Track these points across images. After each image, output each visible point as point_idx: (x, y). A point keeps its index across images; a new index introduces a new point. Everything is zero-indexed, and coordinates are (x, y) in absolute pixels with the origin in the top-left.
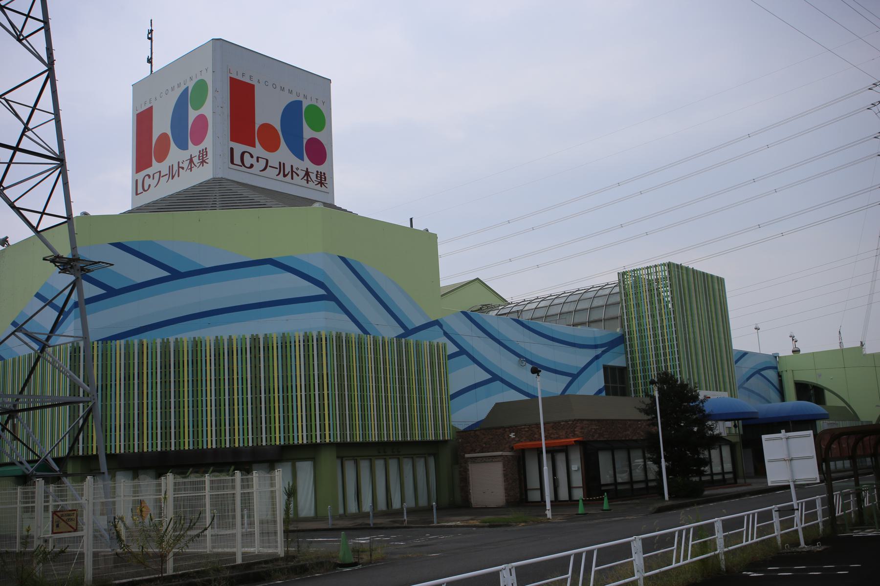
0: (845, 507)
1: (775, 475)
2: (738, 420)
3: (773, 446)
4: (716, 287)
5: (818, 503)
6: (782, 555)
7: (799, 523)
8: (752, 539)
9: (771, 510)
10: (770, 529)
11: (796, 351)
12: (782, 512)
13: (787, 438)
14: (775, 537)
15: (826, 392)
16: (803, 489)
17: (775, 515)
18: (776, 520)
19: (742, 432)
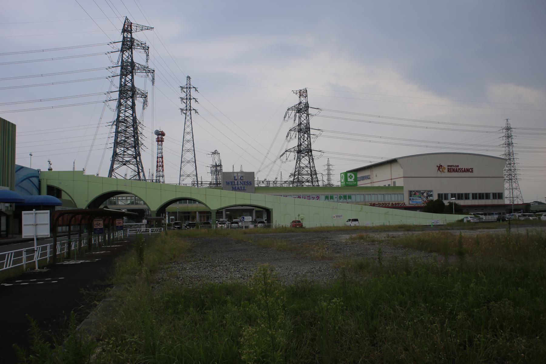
0: (62, 249)
1: (27, 232)
2: (13, 203)
3: (27, 217)
4: (11, 129)
5: (48, 247)
6: (26, 274)
7: (37, 257)
8: (9, 266)
9: (22, 251)
10: (21, 260)
11: (50, 169)
12: (28, 252)
13: (36, 214)
14: (23, 265)
16: (41, 240)
17: (24, 253)
18: (24, 256)
19: (14, 209)
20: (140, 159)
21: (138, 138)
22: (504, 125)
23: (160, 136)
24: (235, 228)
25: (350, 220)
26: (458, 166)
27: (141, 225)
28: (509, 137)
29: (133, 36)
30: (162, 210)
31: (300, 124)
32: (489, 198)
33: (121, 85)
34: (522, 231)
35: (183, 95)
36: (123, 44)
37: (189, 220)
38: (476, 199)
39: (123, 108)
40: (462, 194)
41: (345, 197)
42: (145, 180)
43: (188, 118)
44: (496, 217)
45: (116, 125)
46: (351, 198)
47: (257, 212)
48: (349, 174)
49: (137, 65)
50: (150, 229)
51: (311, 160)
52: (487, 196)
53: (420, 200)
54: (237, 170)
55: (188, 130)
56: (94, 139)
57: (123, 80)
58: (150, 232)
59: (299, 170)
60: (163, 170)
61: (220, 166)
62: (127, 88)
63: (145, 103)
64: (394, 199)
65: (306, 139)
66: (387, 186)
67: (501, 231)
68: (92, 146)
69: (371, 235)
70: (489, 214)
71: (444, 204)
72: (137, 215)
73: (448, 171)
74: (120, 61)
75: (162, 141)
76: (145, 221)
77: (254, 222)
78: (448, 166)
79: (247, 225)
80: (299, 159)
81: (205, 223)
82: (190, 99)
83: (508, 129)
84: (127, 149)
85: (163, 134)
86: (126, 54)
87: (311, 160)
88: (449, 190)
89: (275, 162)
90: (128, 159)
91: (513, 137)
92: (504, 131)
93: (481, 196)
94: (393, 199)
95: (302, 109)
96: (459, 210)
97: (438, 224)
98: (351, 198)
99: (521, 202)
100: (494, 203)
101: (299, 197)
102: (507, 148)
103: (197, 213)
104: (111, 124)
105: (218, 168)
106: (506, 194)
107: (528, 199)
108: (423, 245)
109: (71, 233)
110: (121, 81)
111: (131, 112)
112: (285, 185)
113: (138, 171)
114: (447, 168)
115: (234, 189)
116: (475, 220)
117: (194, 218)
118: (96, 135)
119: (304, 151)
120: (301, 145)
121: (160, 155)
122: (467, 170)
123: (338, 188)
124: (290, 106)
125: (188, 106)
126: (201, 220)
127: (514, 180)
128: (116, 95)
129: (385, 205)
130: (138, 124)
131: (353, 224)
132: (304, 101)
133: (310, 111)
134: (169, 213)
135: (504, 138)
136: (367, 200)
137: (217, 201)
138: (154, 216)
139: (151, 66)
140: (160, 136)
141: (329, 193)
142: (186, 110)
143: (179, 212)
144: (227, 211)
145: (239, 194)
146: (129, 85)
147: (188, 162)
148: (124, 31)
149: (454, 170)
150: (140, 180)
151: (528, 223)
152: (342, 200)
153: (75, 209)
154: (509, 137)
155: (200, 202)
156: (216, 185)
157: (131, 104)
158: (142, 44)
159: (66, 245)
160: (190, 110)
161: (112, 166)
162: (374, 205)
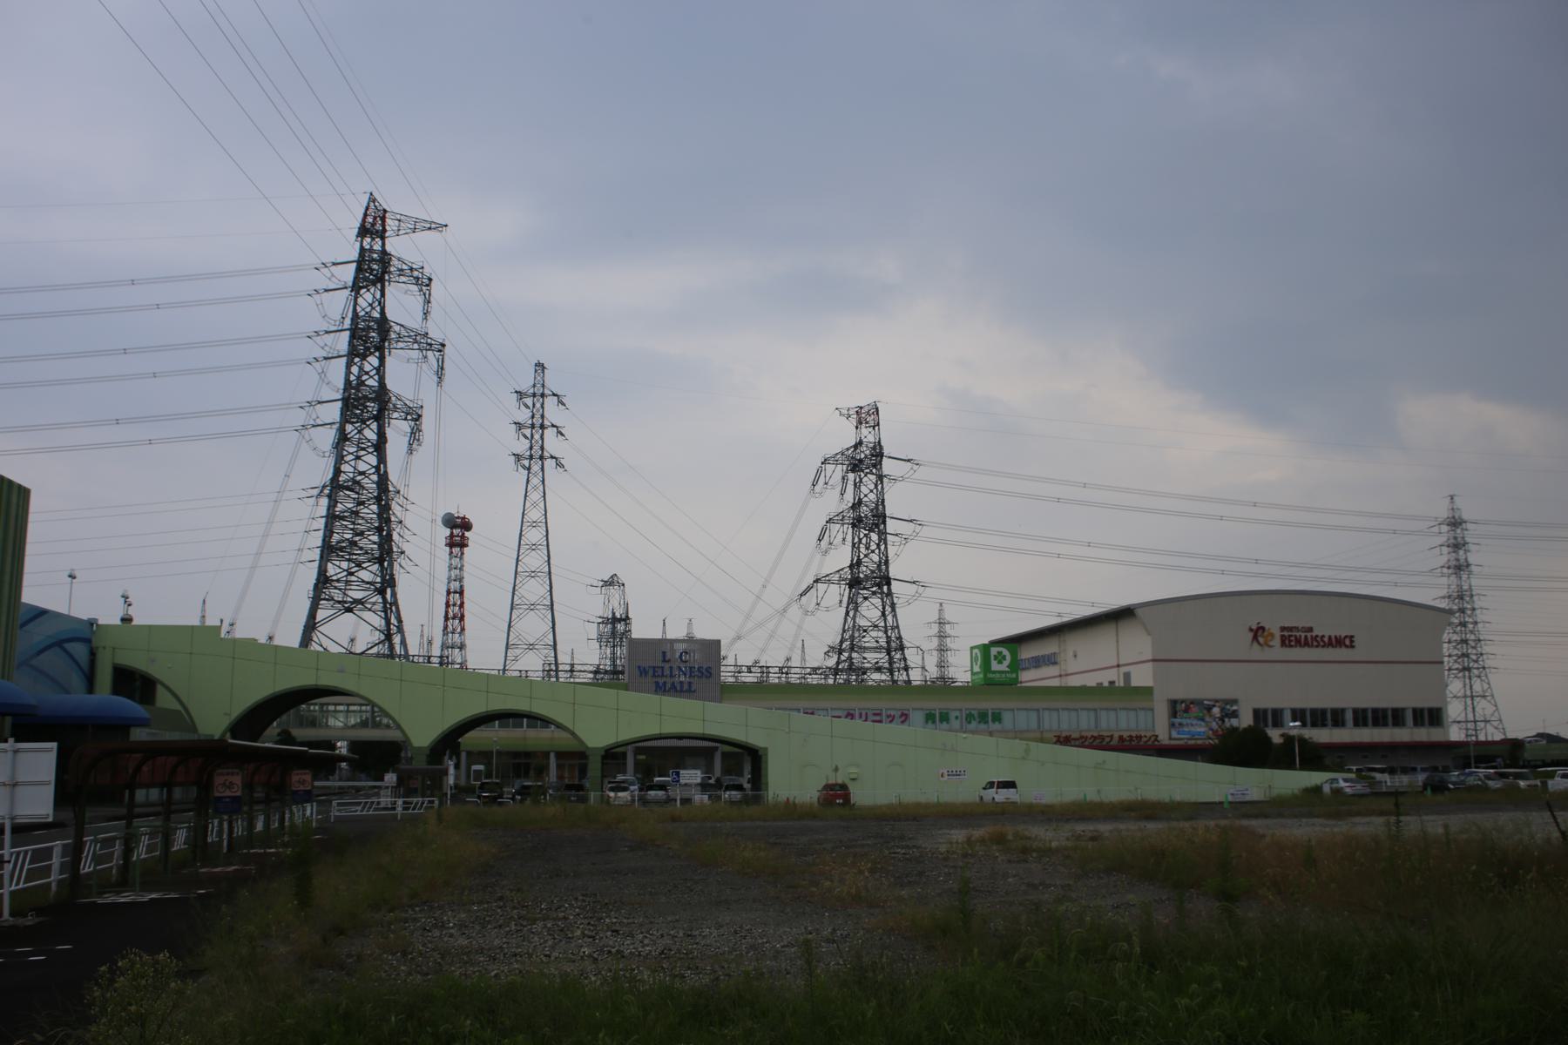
11: (127, 620)
13: (16, 752)
15: (159, 687)
20: (394, 595)
21: (390, 536)
22: (1443, 512)
23: (456, 531)
24: (657, 802)
25: (991, 785)
26: (1310, 630)
27: (379, 787)
28: (1457, 545)
29: (388, 248)
30: (449, 742)
31: (857, 505)
32: (1404, 725)
33: (348, 382)
34: (1435, 824)
35: (524, 416)
36: (359, 270)
37: (526, 775)
38: (1365, 725)
39: (352, 450)
40: (1324, 711)
41: (983, 717)
42: (407, 656)
43: (535, 481)
44: (1421, 778)
45: (329, 496)
46: (1000, 720)
47: (724, 754)
48: (994, 651)
49: (397, 328)
50: (400, 802)
51: (888, 609)
52: (1395, 717)
53: (1201, 728)
54: (676, 632)
55: (535, 514)
56: (265, 536)
57: (355, 370)
58: (399, 809)
59: (852, 638)
60: (463, 629)
61: (626, 619)
62: (365, 391)
63: (415, 435)
64: (1122, 722)
65: (873, 547)
66: (1106, 684)
67: (1370, 826)
68: (258, 554)
69: (1255, 824)
70: (1405, 771)
71: (1268, 739)
72: (377, 756)
73: (1283, 644)
74: (350, 315)
75: (463, 544)
76: (390, 778)
77: (704, 787)
78: (1283, 629)
79: (686, 795)
80: (853, 605)
81: (569, 787)
82: (542, 427)
83: (1455, 523)
84: (359, 565)
85: (466, 525)
86: (367, 297)
87: (888, 609)
88: (1287, 700)
89: (785, 610)
90: (358, 595)
91: (1471, 547)
92: (1445, 528)
93: (1379, 717)
94: (1123, 725)
95: (865, 461)
96: (1313, 757)
97: (1248, 798)
98: (1000, 720)
99: (1498, 737)
100: (1358, 740)
101: (850, 716)
102: (1453, 578)
103: (552, 755)
104: (316, 492)
105: (620, 627)
106: (1454, 710)
107: (1520, 727)
108: (1149, 866)
109: (137, 810)
110: (348, 372)
111: (373, 460)
112: (814, 680)
113: (389, 629)
114: (1278, 634)
115: (660, 689)
116: (1359, 787)
117: (542, 771)
118: (270, 522)
119: (866, 580)
120: (859, 562)
121: (455, 585)
122: (1338, 642)
123: (966, 690)
124: (830, 452)
125: (536, 447)
126: (560, 777)
127: (1476, 672)
128: (333, 412)
129: (1099, 743)
130: (391, 495)
131: (1002, 795)
132: (871, 438)
133: (888, 466)
134: (469, 753)
135: (1445, 550)
136: (1046, 726)
137: (605, 724)
138: (420, 763)
139: (436, 334)
140: (458, 529)
141: (936, 705)
142: (531, 457)
143: (499, 753)
144: (638, 751)
145: (672, 703)
146: (371, 382)
147: (532, 607)
148: (363, 231)
149: (1298, 643)
150: (392, 655)
151: (1514, 799)
152: (974, 725)
153: (195, 737)
154: (1457, 545)
155: (559, 726)
156: (608, 677)
157: (373, 436)
158: (412, 269)
159: (118, 847)
160: (541, 458)
161: (312, 615)
162: (1065, 741)
